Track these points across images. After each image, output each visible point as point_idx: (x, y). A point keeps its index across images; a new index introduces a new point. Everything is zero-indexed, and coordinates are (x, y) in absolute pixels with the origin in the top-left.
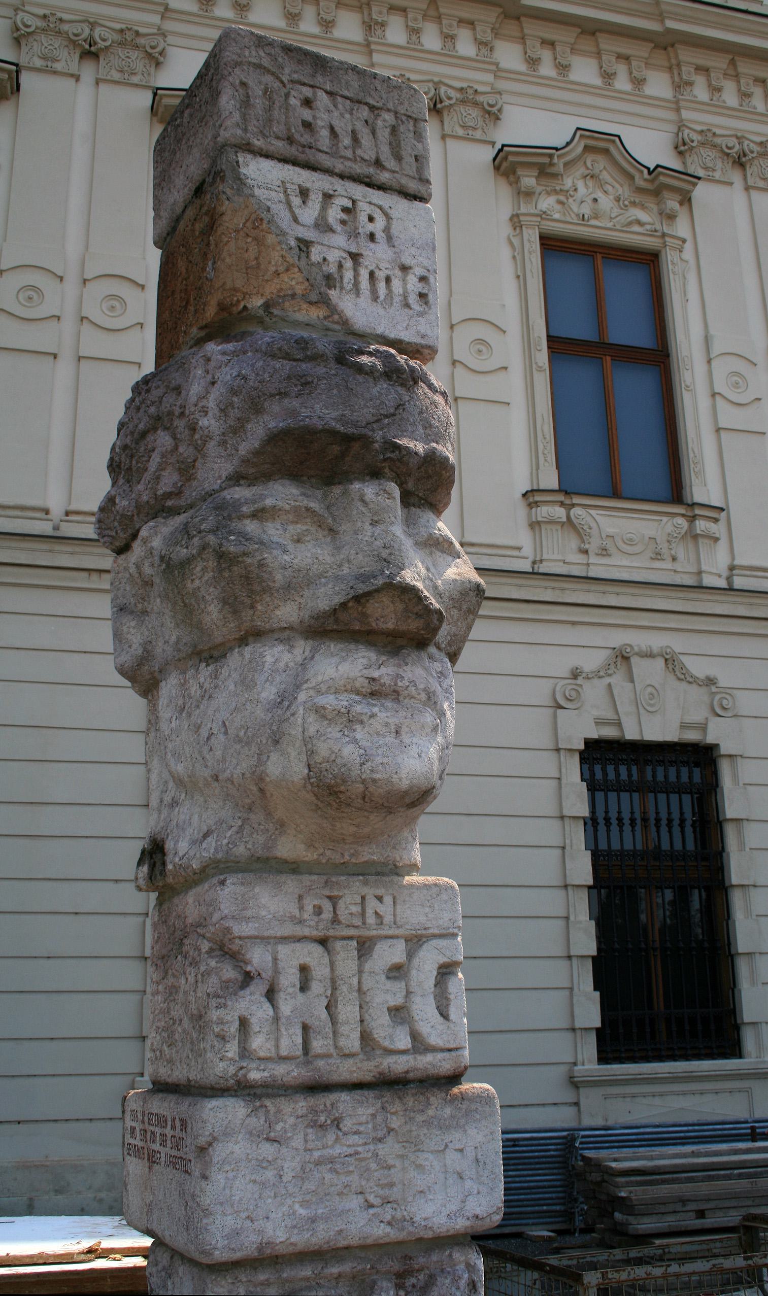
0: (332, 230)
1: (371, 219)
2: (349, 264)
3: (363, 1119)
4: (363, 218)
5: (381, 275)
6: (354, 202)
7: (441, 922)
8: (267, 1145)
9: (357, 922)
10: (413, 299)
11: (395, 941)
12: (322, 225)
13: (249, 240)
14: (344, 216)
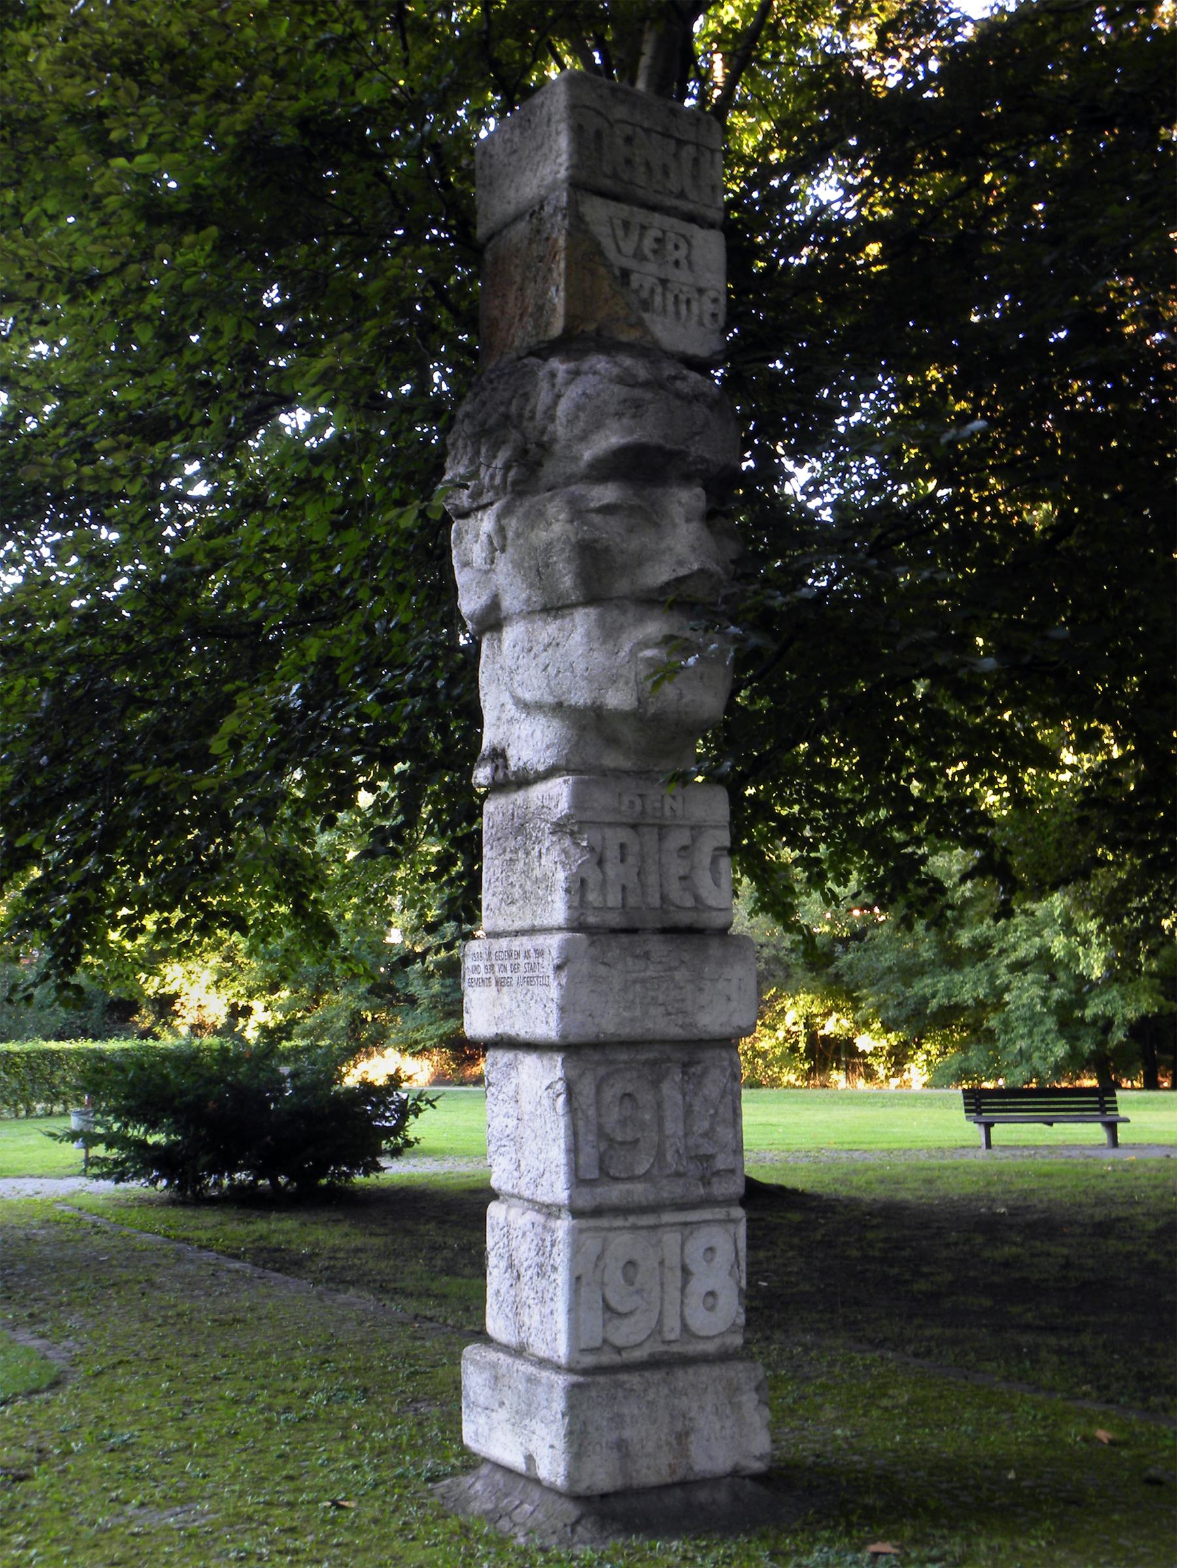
1: (677, 247)
2: (659, 290)
4: (670, 247)
5: (683, 297)
12: (639, 256)
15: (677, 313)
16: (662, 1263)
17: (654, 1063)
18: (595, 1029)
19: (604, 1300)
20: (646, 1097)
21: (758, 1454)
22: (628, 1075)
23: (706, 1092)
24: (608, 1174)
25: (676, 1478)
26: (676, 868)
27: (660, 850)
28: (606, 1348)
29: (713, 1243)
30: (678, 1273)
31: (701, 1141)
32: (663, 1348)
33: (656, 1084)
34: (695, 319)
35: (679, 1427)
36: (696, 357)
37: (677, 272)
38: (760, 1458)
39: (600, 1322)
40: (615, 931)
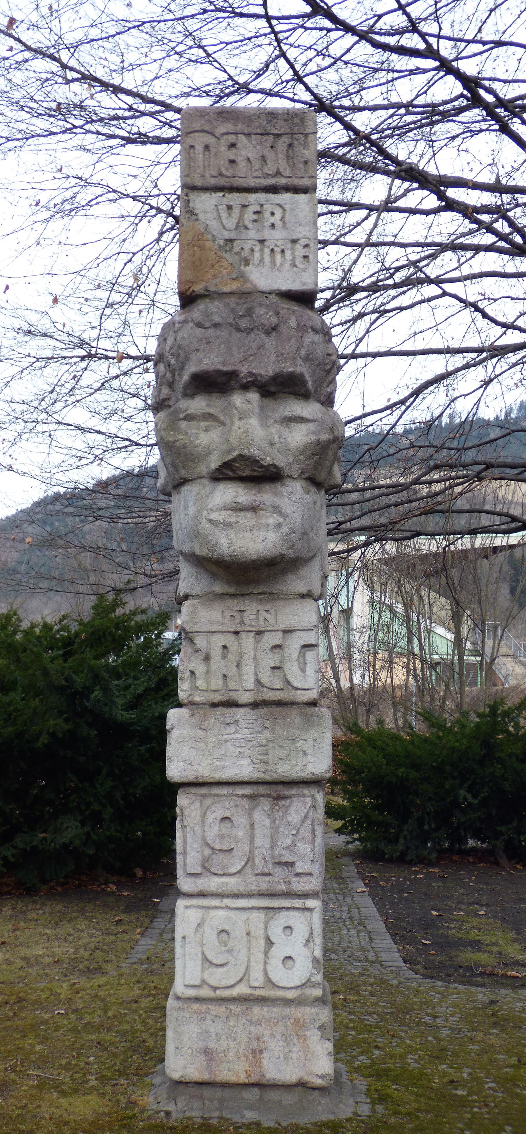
0: (246, 228)
1: (273, 214)
2: (257, 248)
3: (251, 721)
4: (267, 214)
5: (277, 250)
6: (262, 205)
7: (303, 623)
8: (200, 731)
9: (253, 623)
10: (299, 261)
11: (249, 634)
12: (241, 226)
13: (196, 248)
14: (255, 217)
15: (273, 262)
16: (248, 934)
17: (250, 797)
18: (194, 774)
19: (203, 954)
20: (241, 820)
21: (320, 1074)
22: (227, 804)
23: (289, 818)
24: (209, 871)
25: (252, 1080)
26: (270, 660)
27: (255, 649)
28: (205, 986)
29: (290, 923)
30: (262, 942)
31: (283, 852)
32: (249, 991)
33: (250, 813)
34: (288, 263)
35: (255, 1045)
36: (290, 291)
37: (273, 232)
38: (322, 1077)
39: (199, 968)
40: (214, 705)
